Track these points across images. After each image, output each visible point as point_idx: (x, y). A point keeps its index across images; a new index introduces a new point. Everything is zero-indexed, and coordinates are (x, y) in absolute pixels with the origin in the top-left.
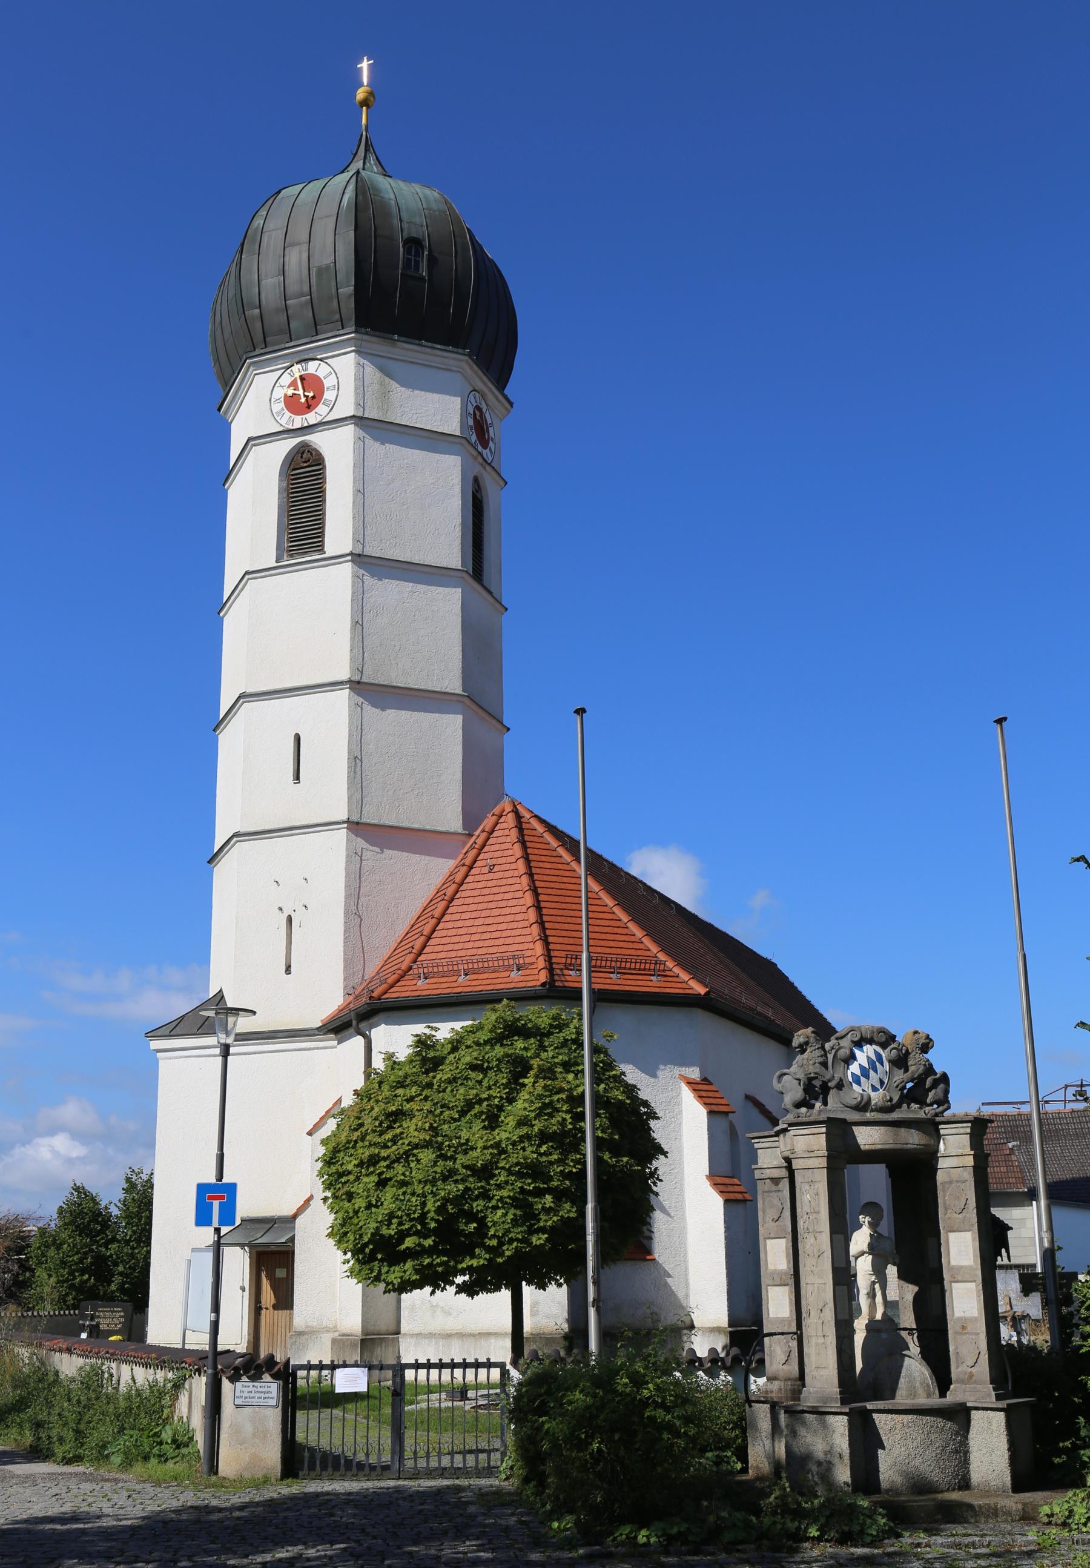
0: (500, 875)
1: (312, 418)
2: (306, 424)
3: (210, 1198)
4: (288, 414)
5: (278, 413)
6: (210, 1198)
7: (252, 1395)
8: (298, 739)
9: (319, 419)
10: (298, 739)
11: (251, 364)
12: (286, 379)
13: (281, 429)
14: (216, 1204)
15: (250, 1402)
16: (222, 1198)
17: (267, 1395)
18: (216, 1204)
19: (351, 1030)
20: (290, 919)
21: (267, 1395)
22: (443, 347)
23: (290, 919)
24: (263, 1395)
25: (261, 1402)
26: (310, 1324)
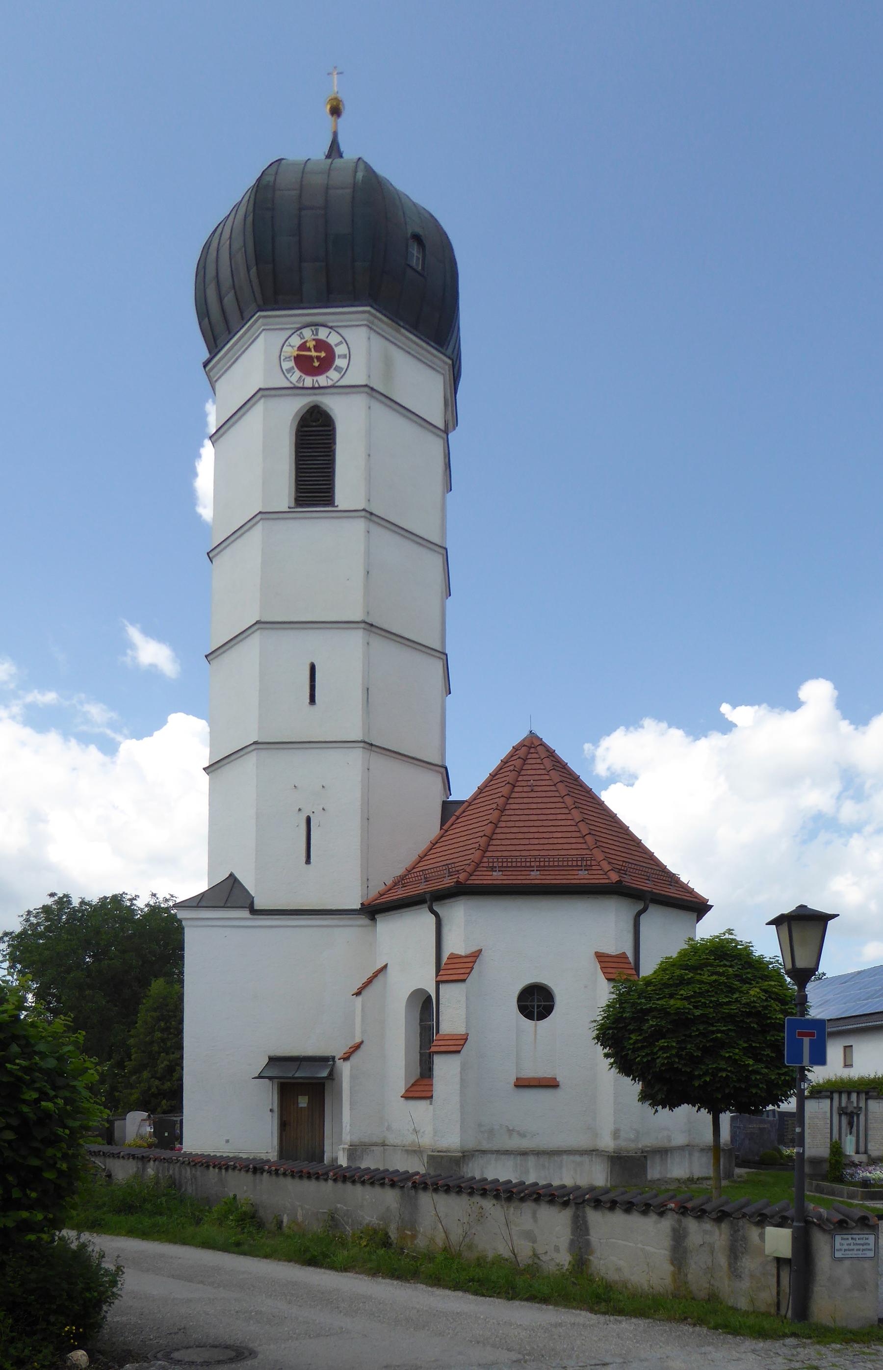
0: (487, 794)
1: (322, 380)
2: (317, 385)
3: (801, 1034)
4: (298, 373)
5: (289, 371)
6: (801, 1034)
7: (852, 1247)
8: (313, 668)
9: (330, 383)
10: (313, 668)
11: (260, 317)
12: (296, 341)
13: (291, 386)
14: (806, 1040)
15: (850, 1254)
16: (812, 1035)
17: (865, 1247)
18: (806, 1040)
19: (426, 905)
20: (308, 820)
21: (865, 1247)
22: (436, 346)
23: (308, 820)
24: (861, 1247)
25: (860, 1254)
26: (363, 1140)
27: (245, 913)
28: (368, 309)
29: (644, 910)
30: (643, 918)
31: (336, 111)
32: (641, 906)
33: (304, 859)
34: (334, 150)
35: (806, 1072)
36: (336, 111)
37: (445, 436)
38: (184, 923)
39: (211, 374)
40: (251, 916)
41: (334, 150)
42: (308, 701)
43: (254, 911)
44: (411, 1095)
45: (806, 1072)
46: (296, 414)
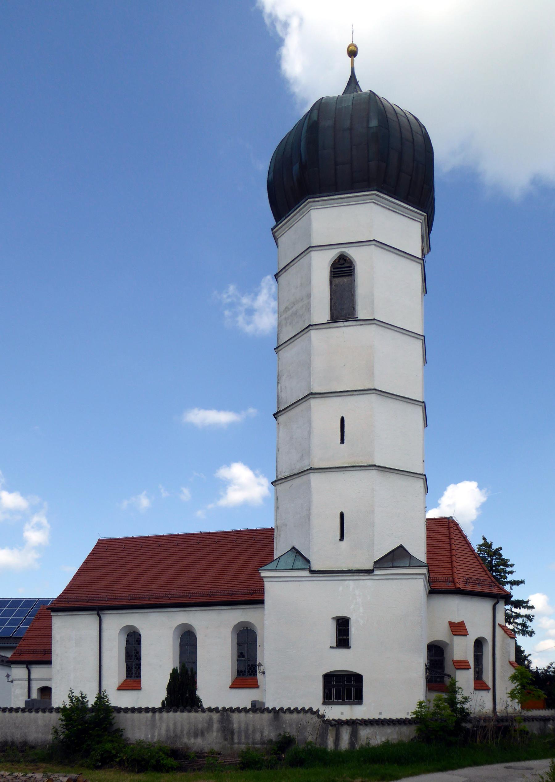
8: (342, 420)
10: (342, 420)
27: (306, 573)
28: (375, 192)
29: (497, 603)
30: (497, 606)
31: (352, 53)
32: (495, 601)
33: (339, 537)
34: (353, 82)
35: (63, 718)
36: (352, 53)
37: (422, 262)
38: (265, 580)
39: (276, 234)
40: (310, 575)
41: (353, 82)
42: (340, 442)
43: (312, 572)
44: (234, 686)
45: (63, 718)
46: (332, 259)
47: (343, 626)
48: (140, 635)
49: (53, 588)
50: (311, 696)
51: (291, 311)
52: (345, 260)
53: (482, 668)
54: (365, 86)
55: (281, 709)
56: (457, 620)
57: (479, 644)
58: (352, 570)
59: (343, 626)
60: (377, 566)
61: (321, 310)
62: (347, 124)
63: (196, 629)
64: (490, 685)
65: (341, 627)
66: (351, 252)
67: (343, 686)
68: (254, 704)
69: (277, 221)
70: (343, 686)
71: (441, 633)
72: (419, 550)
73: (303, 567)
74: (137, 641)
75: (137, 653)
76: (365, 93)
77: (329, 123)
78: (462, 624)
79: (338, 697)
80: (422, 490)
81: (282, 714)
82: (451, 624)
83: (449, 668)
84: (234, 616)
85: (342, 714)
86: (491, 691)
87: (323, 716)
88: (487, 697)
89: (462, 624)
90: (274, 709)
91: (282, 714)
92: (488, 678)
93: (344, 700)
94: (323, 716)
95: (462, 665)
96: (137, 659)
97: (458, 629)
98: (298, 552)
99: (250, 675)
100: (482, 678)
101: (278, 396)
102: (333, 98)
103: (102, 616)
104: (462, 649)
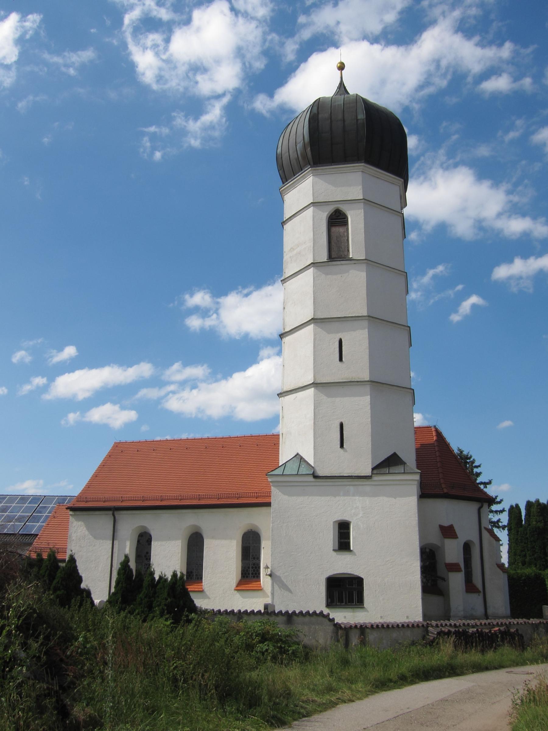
30: (482, 510)
34: (342, 87)
41: (342, 87)
47: (343, 529)
48: (150, 536)
49: (72, 487)
50: (315, 600)
51: (295, 252)
52: (340, 213)
53: (471, 571)
54: (352, 90)
55: (294, 612)
56: (446, 524)
57: (467, 547)
58: (352, 476)
59: (343, 529)
60: (375, 472)
61: (356, 220)
62: (340, 117)
63: (349, 571)
64: (479, 586)
65: (342, 531)
66: (343, 208)
67: (345, 590)
68: (266, 607)
69: (283, 183)
70: (345, 590)
71: (435, 538)
72: (409, 456)
73: (308, 473)
74: (148, 541)
75: (147, 553)
76: (353, 95)
77: (327, 115)
78: (451, 527)
79: (341, 601)
80: (411, 402)
81: (295, 618)
82: (442, 528)
83: (441, 570)
84: (244, 520)
85: (345, 617)
86: (482, 594)
87: (333, 620)
88: (476, 600)
89: (451, 527)
90: (287, 612)
91: (295, 618)
92: (477, 581)
93: (346, 603)
94: (333, 620)
95: (453, 567)
96: (147, 559)
97: (448, 532)
98: (301, 458)
99: (254, 577)
100: (472, 580)
101: (284, 319)
102: (329, 98)
103: (116, 516)
104: (452, 552)
